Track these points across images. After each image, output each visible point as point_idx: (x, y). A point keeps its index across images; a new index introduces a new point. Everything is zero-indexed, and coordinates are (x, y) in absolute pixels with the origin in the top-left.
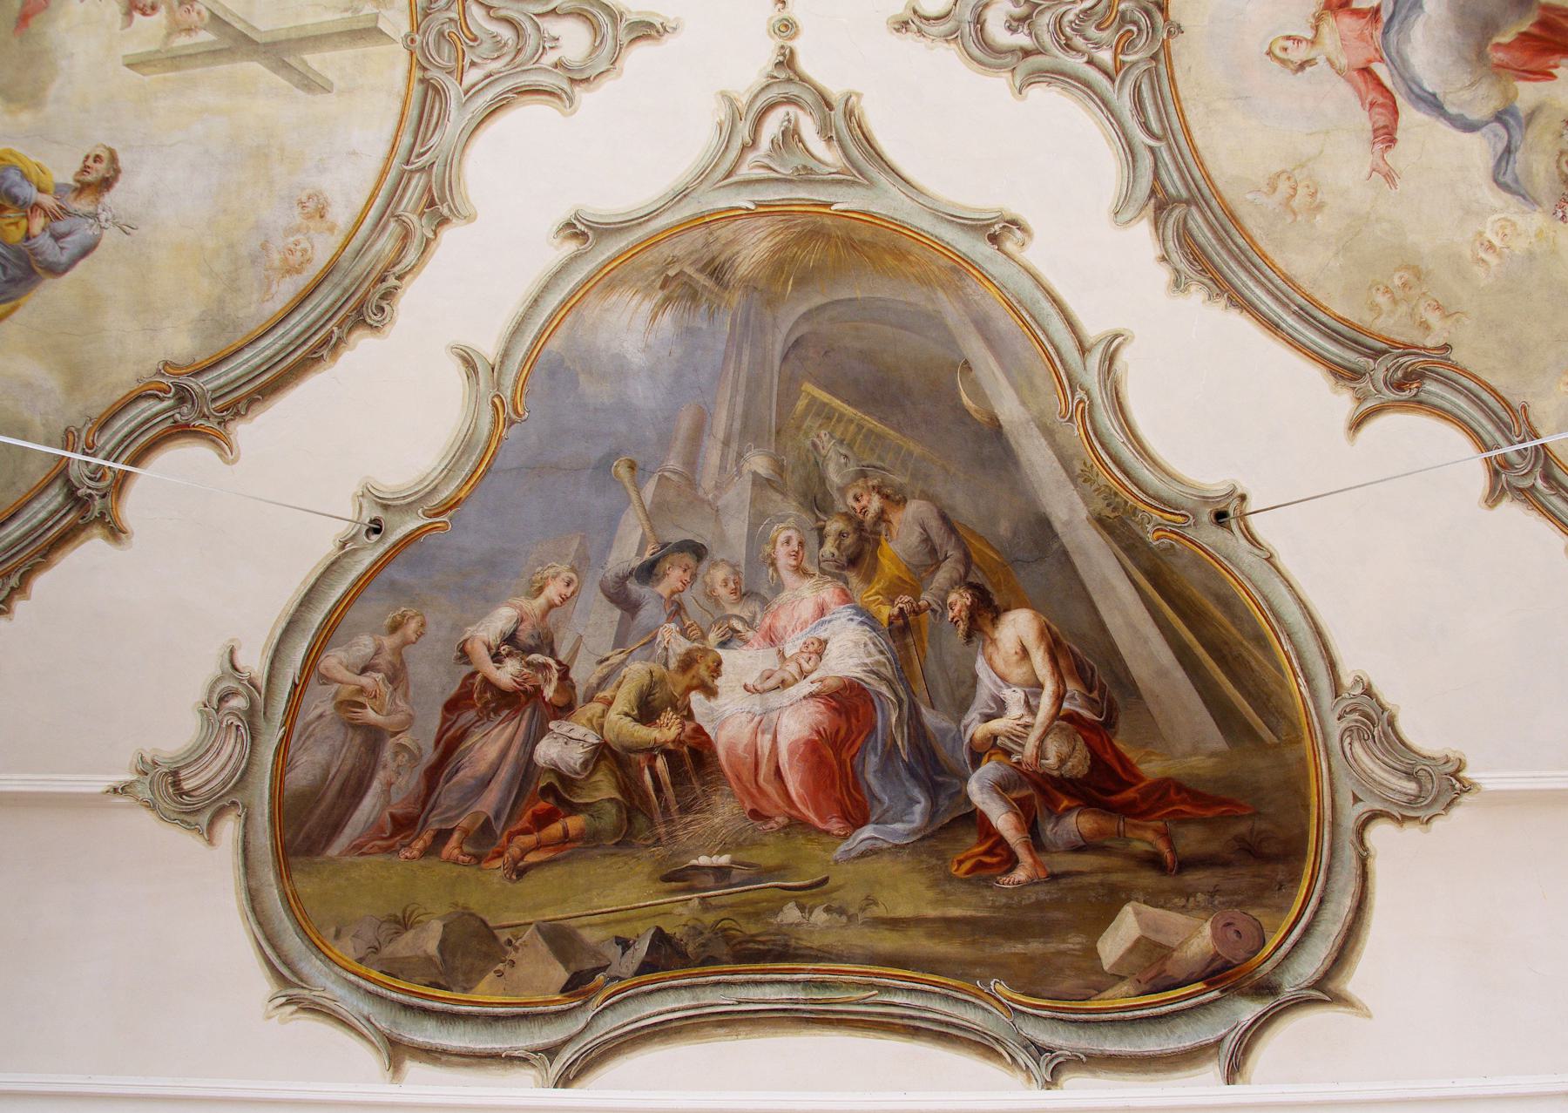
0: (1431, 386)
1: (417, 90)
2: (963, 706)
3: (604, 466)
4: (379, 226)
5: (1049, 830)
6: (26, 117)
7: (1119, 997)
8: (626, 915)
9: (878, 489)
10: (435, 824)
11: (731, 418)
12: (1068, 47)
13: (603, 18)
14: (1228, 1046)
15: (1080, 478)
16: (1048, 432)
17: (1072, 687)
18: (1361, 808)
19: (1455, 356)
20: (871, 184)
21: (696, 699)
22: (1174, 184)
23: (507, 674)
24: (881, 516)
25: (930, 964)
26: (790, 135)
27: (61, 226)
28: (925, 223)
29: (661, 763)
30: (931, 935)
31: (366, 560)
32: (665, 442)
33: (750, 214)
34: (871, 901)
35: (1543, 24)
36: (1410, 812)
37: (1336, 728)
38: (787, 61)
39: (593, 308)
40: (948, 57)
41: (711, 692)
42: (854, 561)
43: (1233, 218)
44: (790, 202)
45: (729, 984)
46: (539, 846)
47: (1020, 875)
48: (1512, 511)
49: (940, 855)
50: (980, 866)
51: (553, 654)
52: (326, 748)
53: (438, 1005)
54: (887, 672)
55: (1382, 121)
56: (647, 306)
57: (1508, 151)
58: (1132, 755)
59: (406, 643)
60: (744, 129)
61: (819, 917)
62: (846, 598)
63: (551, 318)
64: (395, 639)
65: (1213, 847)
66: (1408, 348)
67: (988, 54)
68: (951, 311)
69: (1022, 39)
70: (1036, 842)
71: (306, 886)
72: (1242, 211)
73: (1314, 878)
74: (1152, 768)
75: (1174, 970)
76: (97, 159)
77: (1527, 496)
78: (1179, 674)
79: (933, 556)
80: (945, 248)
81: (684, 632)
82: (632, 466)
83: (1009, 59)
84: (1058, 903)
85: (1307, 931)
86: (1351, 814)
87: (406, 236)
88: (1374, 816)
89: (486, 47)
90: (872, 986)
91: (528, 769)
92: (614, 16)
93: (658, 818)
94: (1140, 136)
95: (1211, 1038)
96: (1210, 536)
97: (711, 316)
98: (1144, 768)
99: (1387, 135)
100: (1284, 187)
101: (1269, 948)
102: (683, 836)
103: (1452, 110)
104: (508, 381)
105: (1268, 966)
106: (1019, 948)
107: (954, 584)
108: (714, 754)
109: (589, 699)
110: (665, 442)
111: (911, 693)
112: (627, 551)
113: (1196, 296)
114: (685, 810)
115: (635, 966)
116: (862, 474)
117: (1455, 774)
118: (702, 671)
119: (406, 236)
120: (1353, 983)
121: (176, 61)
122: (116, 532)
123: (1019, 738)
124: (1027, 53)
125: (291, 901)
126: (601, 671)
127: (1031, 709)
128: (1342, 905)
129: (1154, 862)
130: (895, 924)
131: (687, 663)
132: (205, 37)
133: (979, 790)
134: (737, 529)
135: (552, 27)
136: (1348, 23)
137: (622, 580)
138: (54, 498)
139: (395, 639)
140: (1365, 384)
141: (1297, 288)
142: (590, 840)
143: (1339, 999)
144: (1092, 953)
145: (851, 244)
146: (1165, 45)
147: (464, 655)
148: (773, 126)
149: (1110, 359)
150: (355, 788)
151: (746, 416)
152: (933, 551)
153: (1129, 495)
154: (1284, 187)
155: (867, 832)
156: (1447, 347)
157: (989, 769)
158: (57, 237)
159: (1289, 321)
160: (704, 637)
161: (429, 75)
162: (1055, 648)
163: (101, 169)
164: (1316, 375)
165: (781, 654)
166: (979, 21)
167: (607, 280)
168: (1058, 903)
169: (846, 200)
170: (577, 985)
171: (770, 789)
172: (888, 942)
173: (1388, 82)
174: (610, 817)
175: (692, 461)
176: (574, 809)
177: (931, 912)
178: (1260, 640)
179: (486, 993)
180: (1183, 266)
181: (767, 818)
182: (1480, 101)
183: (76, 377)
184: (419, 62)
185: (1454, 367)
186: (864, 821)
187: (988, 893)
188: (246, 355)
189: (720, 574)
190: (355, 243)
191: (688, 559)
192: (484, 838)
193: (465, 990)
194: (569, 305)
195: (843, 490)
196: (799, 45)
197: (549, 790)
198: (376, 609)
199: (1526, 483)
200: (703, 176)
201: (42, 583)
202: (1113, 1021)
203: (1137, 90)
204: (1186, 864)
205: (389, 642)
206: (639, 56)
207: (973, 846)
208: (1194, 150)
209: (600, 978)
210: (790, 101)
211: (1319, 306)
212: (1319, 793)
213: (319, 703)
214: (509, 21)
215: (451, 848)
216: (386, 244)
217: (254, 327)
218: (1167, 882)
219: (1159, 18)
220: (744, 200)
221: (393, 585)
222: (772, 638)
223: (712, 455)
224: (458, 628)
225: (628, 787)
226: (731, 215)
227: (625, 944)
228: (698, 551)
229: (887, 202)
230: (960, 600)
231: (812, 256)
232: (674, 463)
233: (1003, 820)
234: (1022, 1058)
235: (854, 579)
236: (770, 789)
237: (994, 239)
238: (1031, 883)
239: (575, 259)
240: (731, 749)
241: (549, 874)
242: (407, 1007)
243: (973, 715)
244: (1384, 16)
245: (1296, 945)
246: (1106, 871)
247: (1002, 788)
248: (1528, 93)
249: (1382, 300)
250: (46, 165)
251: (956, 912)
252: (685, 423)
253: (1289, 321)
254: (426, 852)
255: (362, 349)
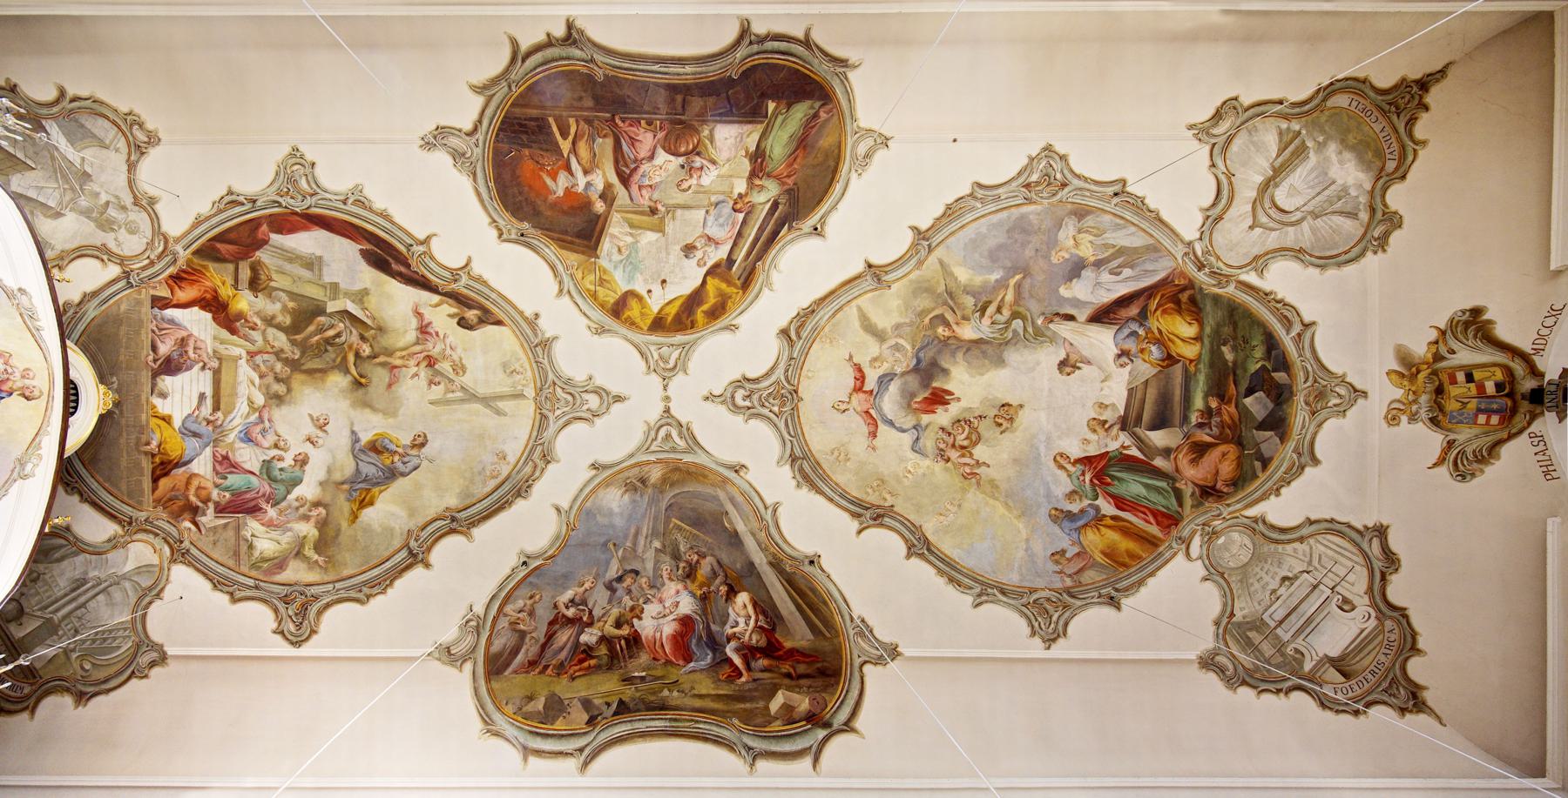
0: (886, 519)
1: (538, 417)
2: (724, 623)
3: (605, 544)
4: (526, 463)
5: (753, 664)
6: (391, 420)
7: (776, 726)
8: (610, 693)
9: (697, 553)
10: (544, 663)
11: (648, 529)
12: (763, 406)
13: (604, 394)
14: (814, 749)
15: (764, 549)
16: (753, 535)
17: (761, 617)
18: (861, 659)
19: (895, 509)
20: (695, 453)
21: (635, 621)
22: (798, 452)
23: (571, 613)
24: (698, 562)
25: (713, 712)
26: (668, 436)
27: (406, 459)
28: (713, 466)
29: (623, 642)
30: (713, 701)
31: (521, 575)
32: (626, 537)
33: (654, 462)
34: (693, 688)
35: (932, 394)
36: (879, 661)
37: (852, 633)
38: (667, 410)
39: (601, 493)
40: (722, 409)
41: (640, 618)
42: (688, 576)
43: (818, 464)
44: (668, 459)
45: (643, 720)
46: (580, 670)
47: (743, 679)
48: (915, 561)
49: (717, 673)
50: (730, 676)
51: (587, 606)
52: (505, 638)
53: (542, 731)
54: (699, 612)
55: (872, 430)
56: (620, 492)
57: (918, 439)
58: (781, 640)
59: (535, 602)
60: (653, 434)
61: (675, 694)
62: (686, 588)
63: (587, 495)
64: (532, 601)
65: (809, 671)
66: (879, 507)
67: (736, 409)
68: (722, 495)
69: (747, 403)
70: (749, 669)
71: (495, 685)
72: (822, 462)
73: (844, 683)
74: (788, 644)
75: (796, 716)
76: (419, 436)
77: (921, 556)
78: (797, 614)
79: (715, 574)
80: (721, 475)
81: (631, 599)
82: (615, 545)
83: (742, 410)
84: (756, 690)
85: (842, 703)
86: (857, 662)
87: (535, 467)
88: (865, 662)
89: (563, 402)
90: (692, 720)
91: (577, 644)
92: (608, 393)
93: (622, 660)
94: (787, 436)
95: (807, 745)
96: (807, 568)
97: (641, 496)
98: (785, 644)
99: (873, 435)
100: (836, 453)
101: (829, 708)
102: (630, 666)
103: (898, 425)
104: (572, 516)
105: (828, 716)
106: (742, 706)
107: (721, 584)
108: (641, 639)
109: (599, 620)
110: (626, 537)
111: (707, 619)
112: (613, 572)
113: (805, 490)
114: (630, 657)
115: (612, 713)
116: (691, 548)
117: (895, 649)
118: (637, 611)
119: (535, 467)
120: (858, 724)
121: (448, 402)
122: (427, 566)
123: (743, 634)
124: (749, 408)
125: (490, 692)
126: (604, 611)
127: (747, 625)
128: (855, 693)
129: (788, 676)
130: (700, 696)
131: (632, 609)
132: (459, 394)
133: (729, 650)
134: (650, 565)
135: (586, 396)
136: (861, 396)
137: (611, 582)
138: (404, 553)
139: (532, 601)
140: (863, 519)
141: (840, 487)
142: (598, 667)
143: (853, 730)
144: (767, 708)
145: (689, 473)
146: (796, 405)
147: (555, 606)
148: (662, 433)
149: (775, 511)
150: (515, 652)
151: (653, 529)
152: (715, 573)
153: (781, 555)
154: (836, 453)
155: (692, 664)
156: (892, 506)
157: (733, 644)
158: (404, 463)
159: (837, 498)
160: (638, 600)
161: (543, 411)
162: (755, 605)
163: (420, 440)
164: (846, 516)
165: (664, 606)
166: (733, 397)
167: (607, 483)
168: (756, 690)
169: (687, 458)
170: (591, 721)
171: (660, 650)
172: (698, 703)
173: (875, 416)
174: (605, 660)
175: (635, 544)
176: (593, 657)
177: (713, 692)
178: (825, 603)
179: (560, 725)
180: (801, 480)
181: (658, 660)
182: (909, 422)
183: (412, 512)
184: (539, 407)
185: (895, 513)
186: (691, 661)
187: (733, 686)
188: (477, 506)
189: (644, 580)
190: (516, 469)
191: (633, 575)
192: (561, 669)
193: (552, 724)
194: (593, 491)
195: (685, 553)
196: (671, 405)
197: (584, 651)
198: (525, 591)
199: (921, 552)
200: (639, 449)
201: (398, 583)
202: (774, 737)
203: (786, 420)
204: (800, 677)
205: (529, 602)
206: (616, 407)
207: (727, 669)
208: (805, 441)
209: (599, 718)
210: (668, 424)
211: (847, 492)
212: (846, 654)
213: (503, 623)
214: (571, 394)
215: (549, 671)
216: (528, 469)
217: (480, 496)
218: (793, 683)
219: (795, 395)
220: (652, 458)
221: (531, 583)
222: (661, 601)
223: (641, 541)
224: (554, 597)
225: (611, 649)
226: (648, 463)
227: (608, 704)
228: (637, 573)
229: (701, 459)
230: (724, 589)
231: (676, 477)
232: (629, 544)
233: (737, 661)
234: (743, 752)
235: (688, 581)
236: (660, 650)
237: (736, 471)
238: (747, 682)
239: (595, 476)
240: (646, 638)
241: (583, 679)
242: (531, 732)
243: (728, 626)
244: (875, 393)
245: (838, 708)
246: (773, 678)
247: (737, 650)
248: (925, 419)
249: (870, 491)
250: (399, 437)
251: (722, 692)
252: (633, 531)
253: (837, 498)
254: (540, 673)
255: (520, 505)
